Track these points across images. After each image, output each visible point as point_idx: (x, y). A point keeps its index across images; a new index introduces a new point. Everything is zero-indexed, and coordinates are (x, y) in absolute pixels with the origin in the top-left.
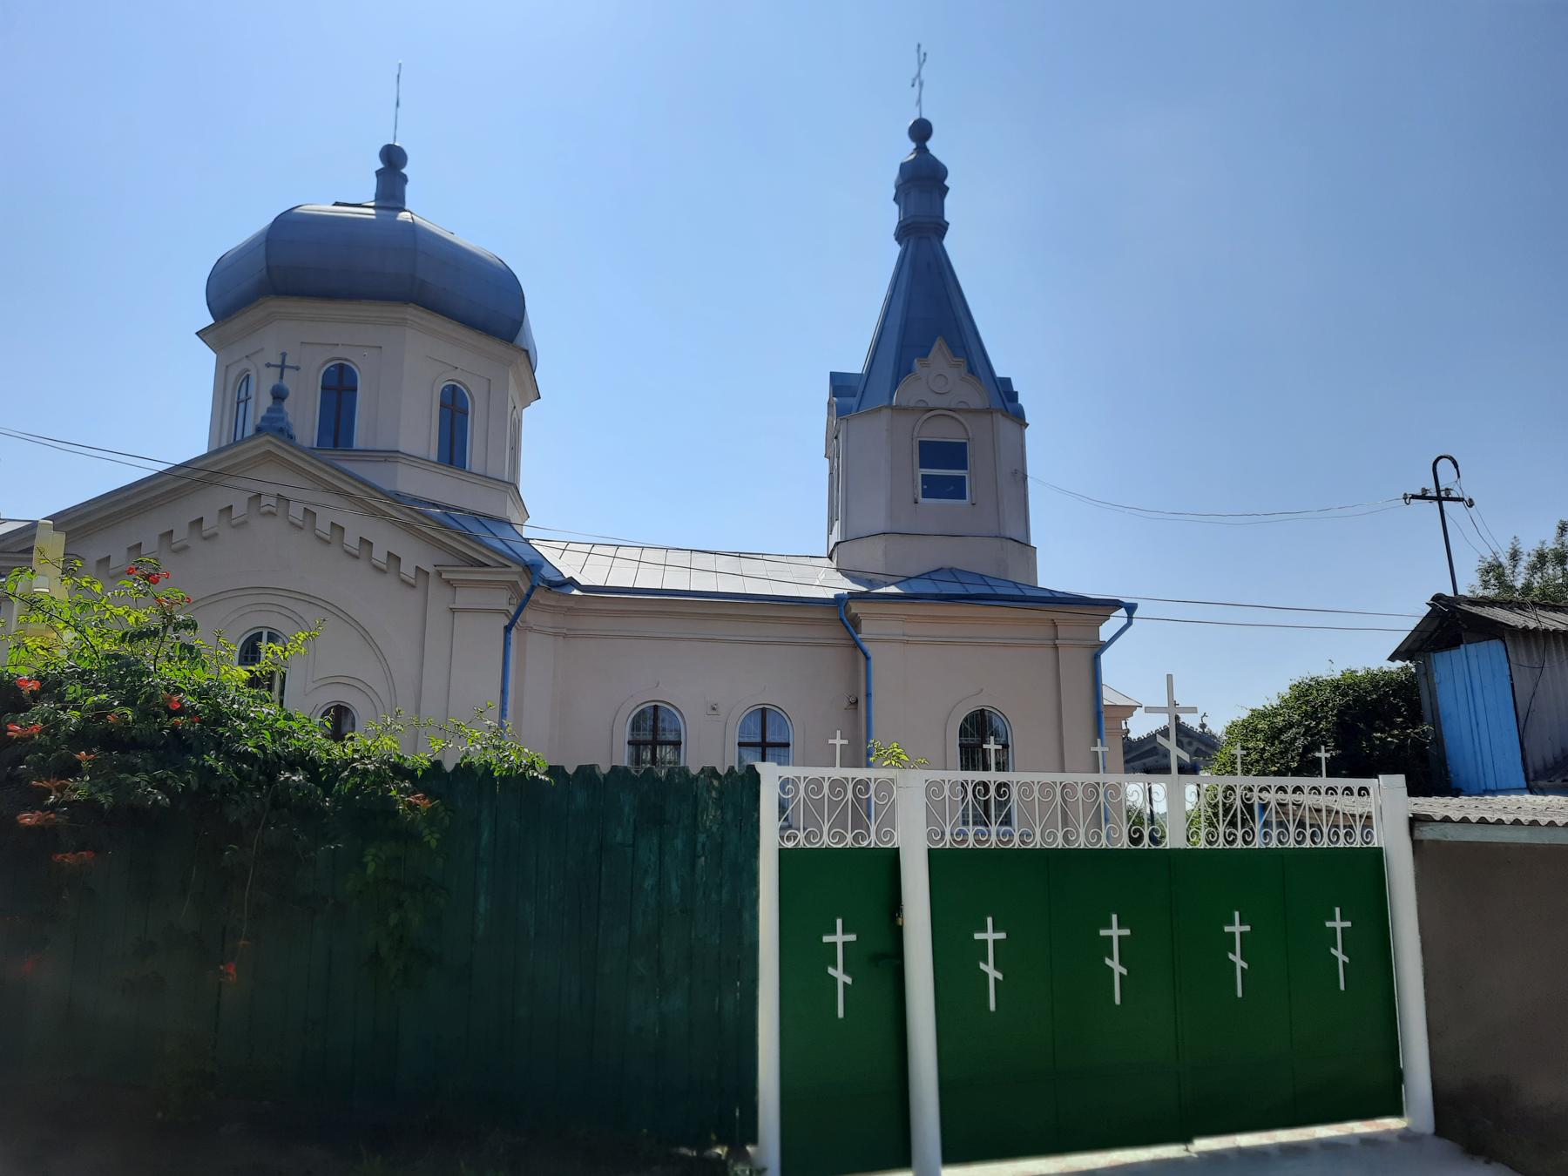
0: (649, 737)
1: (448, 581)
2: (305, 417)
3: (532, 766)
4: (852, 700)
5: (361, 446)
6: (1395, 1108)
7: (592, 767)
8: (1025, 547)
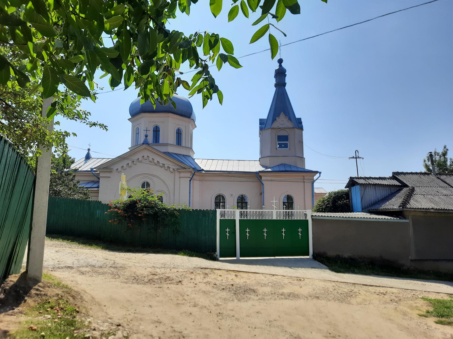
0: (219, 201)
1: (179, 172)
2: (150, 139)
3: (190, 209)
4: (261, 193)
5: (161, 143)
6: (308, 255)
7: (197, 209)
8: (302, 158)
